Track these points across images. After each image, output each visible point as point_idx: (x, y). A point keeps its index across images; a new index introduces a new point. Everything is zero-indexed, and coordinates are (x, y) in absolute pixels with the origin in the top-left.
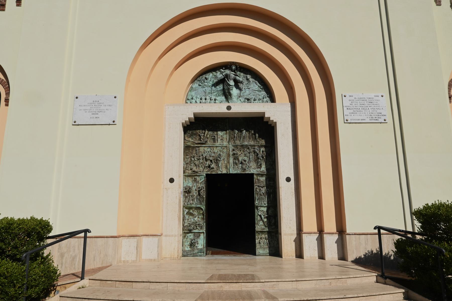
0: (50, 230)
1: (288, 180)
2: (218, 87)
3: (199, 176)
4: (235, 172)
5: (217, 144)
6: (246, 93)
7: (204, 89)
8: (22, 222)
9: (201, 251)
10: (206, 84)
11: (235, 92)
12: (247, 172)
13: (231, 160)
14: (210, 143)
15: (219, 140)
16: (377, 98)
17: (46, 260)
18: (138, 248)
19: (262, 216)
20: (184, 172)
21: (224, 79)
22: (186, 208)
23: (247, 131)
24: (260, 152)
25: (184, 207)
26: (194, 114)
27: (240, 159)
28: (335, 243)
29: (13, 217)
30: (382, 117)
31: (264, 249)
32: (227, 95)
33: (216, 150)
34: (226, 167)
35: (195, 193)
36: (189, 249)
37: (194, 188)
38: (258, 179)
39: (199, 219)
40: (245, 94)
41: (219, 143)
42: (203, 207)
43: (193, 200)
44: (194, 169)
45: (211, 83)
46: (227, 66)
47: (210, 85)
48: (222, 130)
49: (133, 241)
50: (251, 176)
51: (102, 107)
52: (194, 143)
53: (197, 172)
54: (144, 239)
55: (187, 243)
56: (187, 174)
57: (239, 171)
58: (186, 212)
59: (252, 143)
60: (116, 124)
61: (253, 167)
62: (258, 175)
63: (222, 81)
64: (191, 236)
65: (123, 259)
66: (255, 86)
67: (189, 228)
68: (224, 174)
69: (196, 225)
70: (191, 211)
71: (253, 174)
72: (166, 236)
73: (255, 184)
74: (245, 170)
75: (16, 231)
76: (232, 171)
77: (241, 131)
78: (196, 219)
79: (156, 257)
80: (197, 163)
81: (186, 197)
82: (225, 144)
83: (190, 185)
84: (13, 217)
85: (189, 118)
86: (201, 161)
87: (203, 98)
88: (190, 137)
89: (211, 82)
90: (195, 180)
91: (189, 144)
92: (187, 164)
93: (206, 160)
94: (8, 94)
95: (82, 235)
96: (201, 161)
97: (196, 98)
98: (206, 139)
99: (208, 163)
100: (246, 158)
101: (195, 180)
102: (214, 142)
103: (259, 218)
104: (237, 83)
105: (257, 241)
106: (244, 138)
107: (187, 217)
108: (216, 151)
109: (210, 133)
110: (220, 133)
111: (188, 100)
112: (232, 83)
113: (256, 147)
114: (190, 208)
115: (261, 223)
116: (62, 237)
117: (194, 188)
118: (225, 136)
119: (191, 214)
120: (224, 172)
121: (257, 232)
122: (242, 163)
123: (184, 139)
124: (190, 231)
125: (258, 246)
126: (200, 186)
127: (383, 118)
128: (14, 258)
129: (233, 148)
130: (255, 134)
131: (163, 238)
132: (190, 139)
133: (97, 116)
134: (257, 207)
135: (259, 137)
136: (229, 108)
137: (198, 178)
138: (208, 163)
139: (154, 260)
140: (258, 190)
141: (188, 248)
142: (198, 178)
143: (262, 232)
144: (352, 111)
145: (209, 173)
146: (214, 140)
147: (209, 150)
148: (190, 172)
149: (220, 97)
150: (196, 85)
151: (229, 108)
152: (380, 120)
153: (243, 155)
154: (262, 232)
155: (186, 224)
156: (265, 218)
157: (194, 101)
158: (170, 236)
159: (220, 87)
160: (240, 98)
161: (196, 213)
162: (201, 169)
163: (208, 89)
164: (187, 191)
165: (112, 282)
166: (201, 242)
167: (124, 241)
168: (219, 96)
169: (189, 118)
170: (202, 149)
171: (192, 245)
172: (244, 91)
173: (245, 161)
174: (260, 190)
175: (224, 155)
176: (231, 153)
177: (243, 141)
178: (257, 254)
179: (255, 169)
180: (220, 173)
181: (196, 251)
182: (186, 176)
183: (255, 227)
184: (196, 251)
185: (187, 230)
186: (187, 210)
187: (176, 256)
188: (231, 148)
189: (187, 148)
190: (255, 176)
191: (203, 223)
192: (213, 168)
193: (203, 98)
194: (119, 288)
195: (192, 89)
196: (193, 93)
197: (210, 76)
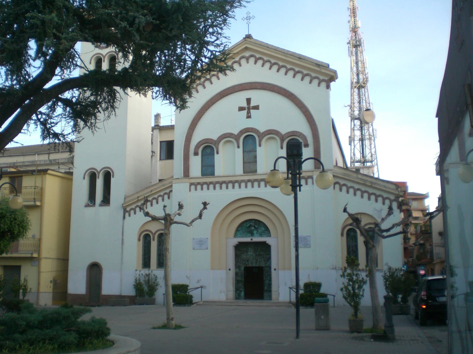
11: (255, 232)
16: (307, 237)
26: (238, 242)
28: (323, 285)
29: (161, 287)
39: (241, 285)
41: (249, 253)
46: (251, 220)
50: (262, 267)
60: (190, 191)
63: (250, 226)
64: (238, 292)
84: (161, 287)
93: (244, 261)
127: (309, 245)
136: (252, 239)
141: (237, 297)
151: (252, 239)
164: (237, 274)
165: (293, 250)
166: (243, 294)
188: (254, 255)
190: (264, 268)
191: (243, 287)
194: (353, 76)
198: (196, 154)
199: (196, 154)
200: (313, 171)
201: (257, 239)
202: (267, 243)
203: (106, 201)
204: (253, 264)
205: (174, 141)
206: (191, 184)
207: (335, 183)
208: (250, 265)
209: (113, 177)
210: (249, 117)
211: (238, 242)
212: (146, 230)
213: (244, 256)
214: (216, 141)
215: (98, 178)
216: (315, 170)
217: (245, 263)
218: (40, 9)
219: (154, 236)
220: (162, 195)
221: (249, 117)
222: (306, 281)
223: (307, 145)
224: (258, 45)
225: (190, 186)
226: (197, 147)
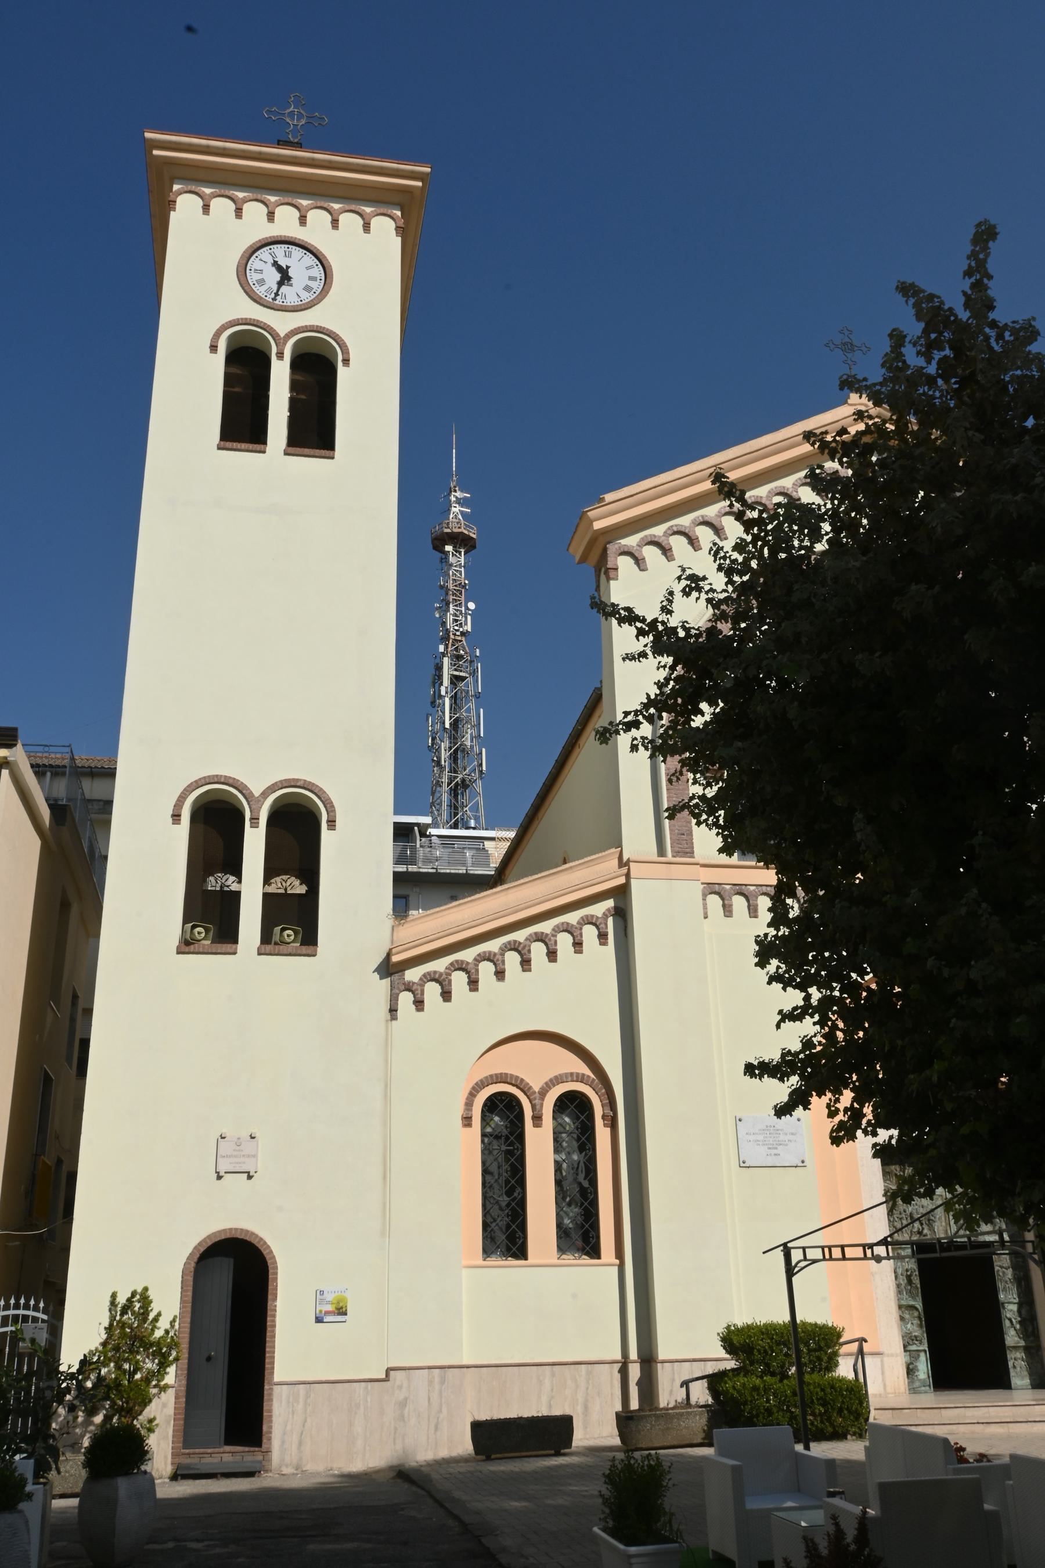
42: (919, 1305)
51: (782, 1137)
72: (888, 1356)
73: (995, 1264)
78: (909, 1326)
105: (1010, 1364)
115: (1012, 1332)
133: (776, 1151)
134: (1003, 1304)
178: (1013, 1386)
212: (501, 1078)
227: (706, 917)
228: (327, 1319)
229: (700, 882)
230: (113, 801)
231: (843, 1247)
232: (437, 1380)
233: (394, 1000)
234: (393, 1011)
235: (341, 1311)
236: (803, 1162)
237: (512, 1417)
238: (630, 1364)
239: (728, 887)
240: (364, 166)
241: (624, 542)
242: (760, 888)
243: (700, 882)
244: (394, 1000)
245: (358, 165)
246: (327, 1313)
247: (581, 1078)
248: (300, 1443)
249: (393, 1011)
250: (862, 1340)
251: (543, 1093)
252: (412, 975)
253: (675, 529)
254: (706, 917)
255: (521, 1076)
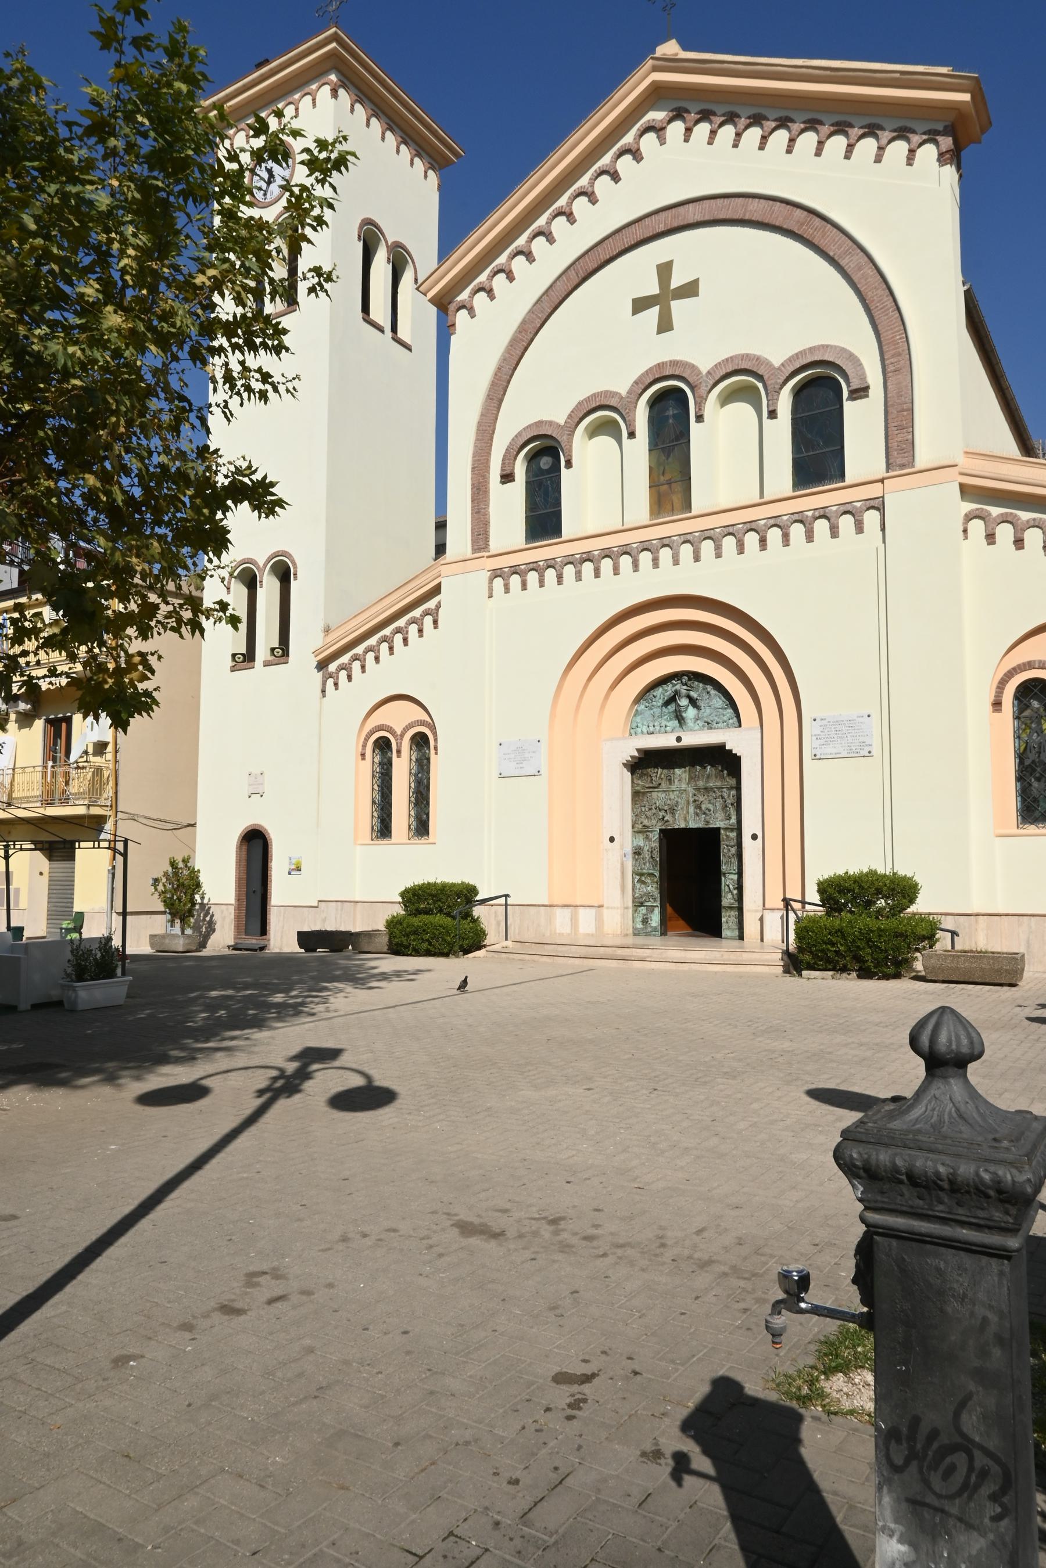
0: (476, 894)
1: (754, 837)
2: (669, 707)
3: (651, 831)
4: (696, 826)
5: (673, 787)
6: (706, 712)
7: (652, 712)
8: (453, 885)
9: (655, 929)
10: (654, 703)
11: (691, 713)
12: (711, 826)
13: (692, 809)
14: (664, 786)
15: (676, 781)
16: (861, 719)
17: (475, 921)
18: (574, 921)
19: (731, 887)
20: (633, 827)
21: (674, 696)
22: (637, 874)
23: (712, 766)
24: (729, 796)
25: (633, 872)
27: (703, 807)
30: (866, 748)
31: (733, 930)
32: (680, 718)
33: (672, 796)
34: (685, 820)
35: (647, 856)
36: (641, 926)
37: (646, 848)
38: (727, 836)
39: (652, 888)
40: (705, 714)
42: (657, 874)
43: (644, 864)
44: (646, 822)
45: (661, 702)
47: (660, 704)
48: (680, 767)
49: (567, 911)
51: (527, 755)
52: (644, 787)
53: (648, 827)
54: (581, 910)
55: (639, 919)
56: (636, 830)
57: (701, 825)
58: (636, 880)
59: (719, 784)
61: (720, 818)
62: (726, 829)
63: (672, 700)
65: (558, 931)
66: (718, 701)
67: (641, 900)
68: (683, 829)
69: (648, 895)
70: (643, 879)
71: (718, 829)
72: (608, 908)
73: (722, 843)
74: (708, 822)
75: (448, 893)
76: (692, 825)
77: (705, 768)
78: (649, 888)
79: (594, 932)
80: (649, 814)
81: (636, 860)
82: (684, 786)
83: (641, 843)
85: (631, 757)
86: (654, 811)
87: (651, 724)
88: (640, 778)
89: (661, 701)
90: (647, 837)
91: (638, 788)
92: (636, 816)
93: (660, 810)
94: (435, 734)
95: (502, 900)
96: (654, 811)
97: (643, 725)
98: (660, 781)
99: (661, 814)
100: (710, 806)
101: (647, 837)
102: (670, 784)
103: (727, 889)
104: (693, 702)
105: (723, 920)
106: (709, 777)
107: (638, 885)
108: (672, 797)
109: (665, 771)
110: (677, 771)
111: (633, 731)
112: (684, 702)
113: (725, 790)
114: (642, 875)
115: (730, 896)
116: (483, 902)
117: (646, 848)
118: (684, 776)
119: (643, 882)
120: (683, 825)
121: (724, 907)
122: (704, 813)
123: (633, 782)
124: (642, 905)
125: (724, 926)
126: (654, 845)
128: (448, 915)
129: (694, 791)
130: (722, 771)
131: (605, 911)
132: (640, 782)
133: (521, 765)
134: (724, 874)
135: (729, 775)
136: (679, 739)
137: (651, 835)
138: (661, 814)
139: (592, 935)
140: (725, 851)
141: (640, 926)
142: (651, 835)
143: (731, 908)
144: (822, 742)
145: (663, 827)
146: (670, 781)
147: (663, 795)
148: (640, 826)
149: (672, 722)
150: (641, 707)
152: (863, 753)
153: (707, 802)
154: (731, 908)
155: (637, 895)
156: (735, 889)
157: (639, 730)
158: (612, 908)
159: (672, 707)
160: (698, 722)
161: (648, 881)
162: (654, 822)
163: (657, 711)
164: (637, 852)
166: (655, 919)
167: (558, 911)
168: (671, 719)
169: (631, 757)
170: (654, 795)
171: (645, 921)
172: (703, 711)
173: (710, 810)
174: (729, 850)
175: (682, 802)
176: (691, 800)
177: (707, 782)
178: (723, 936)
179: (722, 820)
180: (677, 827)
181: (649, 929)
182: (636, 832)
183: (721, 901)
184: (649, 929)
185: (638, 903)
186: (638, 877)
187: (619, 932)
188: (691, 790)
189: (636, 795)
190: (722, 832)
192: (667, 821)
193: (651, 724)
195: (637, 713)
196: (638, 719)
197: (659, 691)
198: (507, 478)
199: (507, 478)
200: (882, 481)
201: (696, 737)
202: (727, 748)
203: (282, 650)
204: (687, 819)
205: (299, 933)
206: (496, 573)
207: (969, 517)
208: (680, 823)
209: (296, 578)
210: (665, 325)
211: (638, 750)
212: (380, 728)
213: (659, 797)
214: (562, 427)
215: (261, 587)
216: (891, 474)
217: (664, 817)
218: (350, 947)
219: (401, 743)
220: (418, 616)
221: (665, 325)
222: (827, 873)
223: (860, 392)
224: (603, 254)
225: (491, 580)
226: (510, 457)
227: (491, 596)
228: (293, 873)
229: (486, 571)
230: (445, 544)
231: (94, 848)
232: (339, 908)
233: (324, 683)
234: (323, 691)
235: (299, 869)
236: (870, 752)
237: (329, 929)
238: (619, 906)
239: (506, 570)
240: (244, 85)
241: (459, 298)
242: (868, 502)
243: (486, 571)
244: (324, 683)
245: (295, 55)
246: (293, 869)
247: (423, 723)
248: (282, 937)
249: (323, 691)
250: (507, 896)
251: (402, 735)
252: (332, 667)
253: (495, 270)
254: (491, 596)
255: (391, 725)
